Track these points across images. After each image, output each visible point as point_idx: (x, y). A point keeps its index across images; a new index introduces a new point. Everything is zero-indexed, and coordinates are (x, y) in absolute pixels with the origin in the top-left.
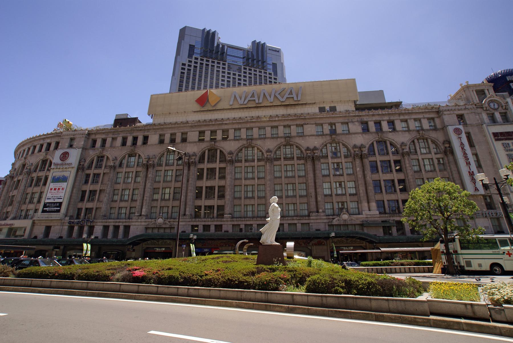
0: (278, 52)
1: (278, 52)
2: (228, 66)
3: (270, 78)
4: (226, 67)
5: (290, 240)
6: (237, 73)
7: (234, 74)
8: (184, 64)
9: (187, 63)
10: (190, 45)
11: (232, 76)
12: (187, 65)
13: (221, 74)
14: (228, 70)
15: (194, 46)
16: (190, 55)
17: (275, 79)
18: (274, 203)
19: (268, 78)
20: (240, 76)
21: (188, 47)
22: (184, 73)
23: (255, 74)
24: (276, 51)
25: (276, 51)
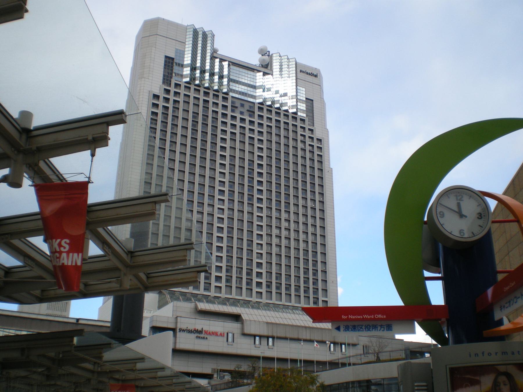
0: (316, 76)
1: (316, 76)
2: (233, 102)
3: (224, 115)
4: (229, 104)
5: (428, 352)
6: (248, 118)
7: (243, 120)
8: (156, 97)
9: (162, 95)
10: (166, 57)
11: (238, 123)
12: (161, 98)
13: (220, 119)
14: (233, 111)
15: (173, 59)
16: (167, 80)
17: (156, 105)
18: (440, 244)
19: (220, 115)
20: (252, 123)
21: (161, 62)
22: (156, 114)
23: (175, 101)
24: (311, 74)
25: (311, 74)
